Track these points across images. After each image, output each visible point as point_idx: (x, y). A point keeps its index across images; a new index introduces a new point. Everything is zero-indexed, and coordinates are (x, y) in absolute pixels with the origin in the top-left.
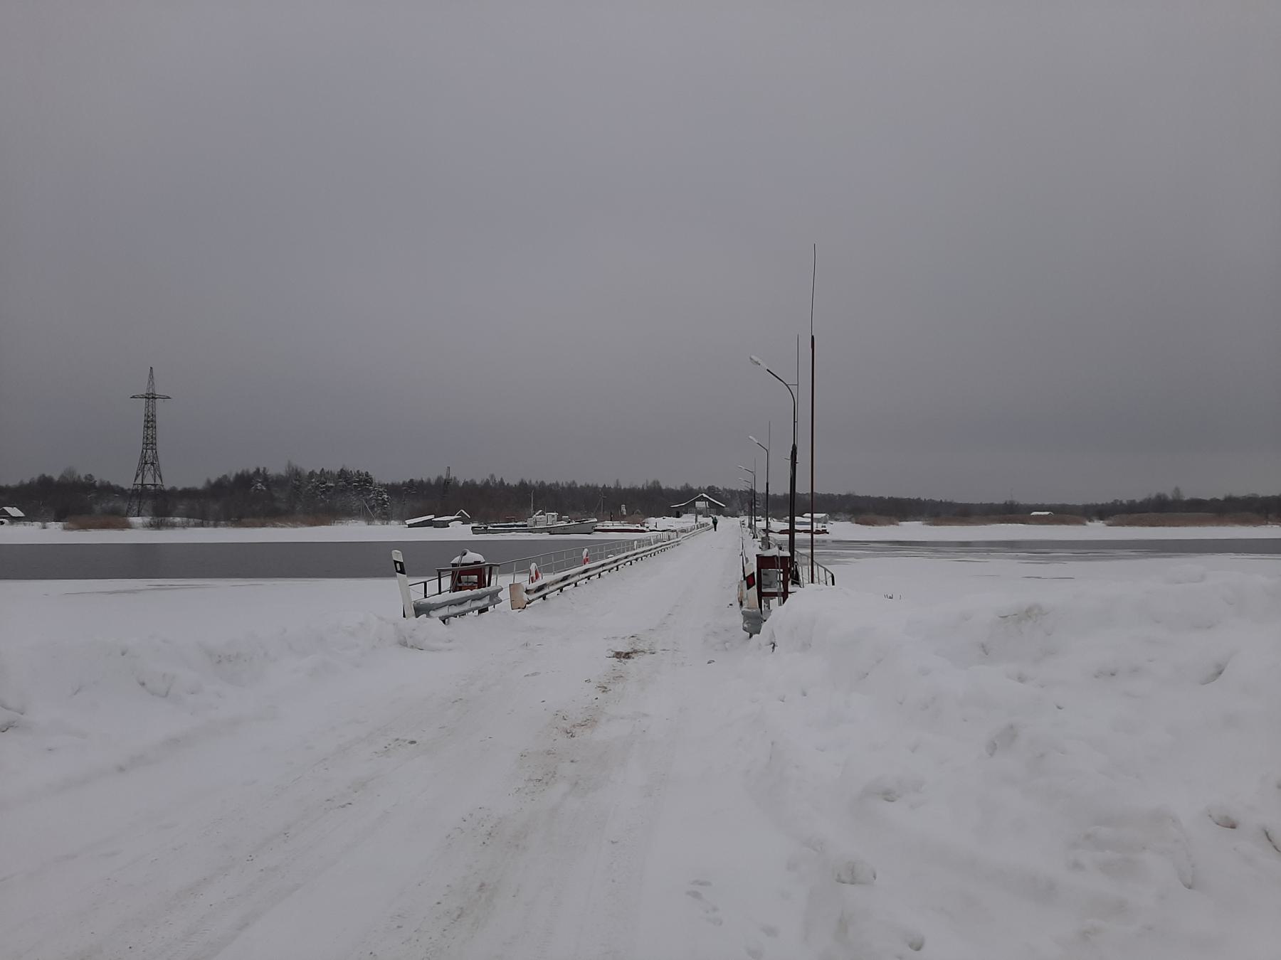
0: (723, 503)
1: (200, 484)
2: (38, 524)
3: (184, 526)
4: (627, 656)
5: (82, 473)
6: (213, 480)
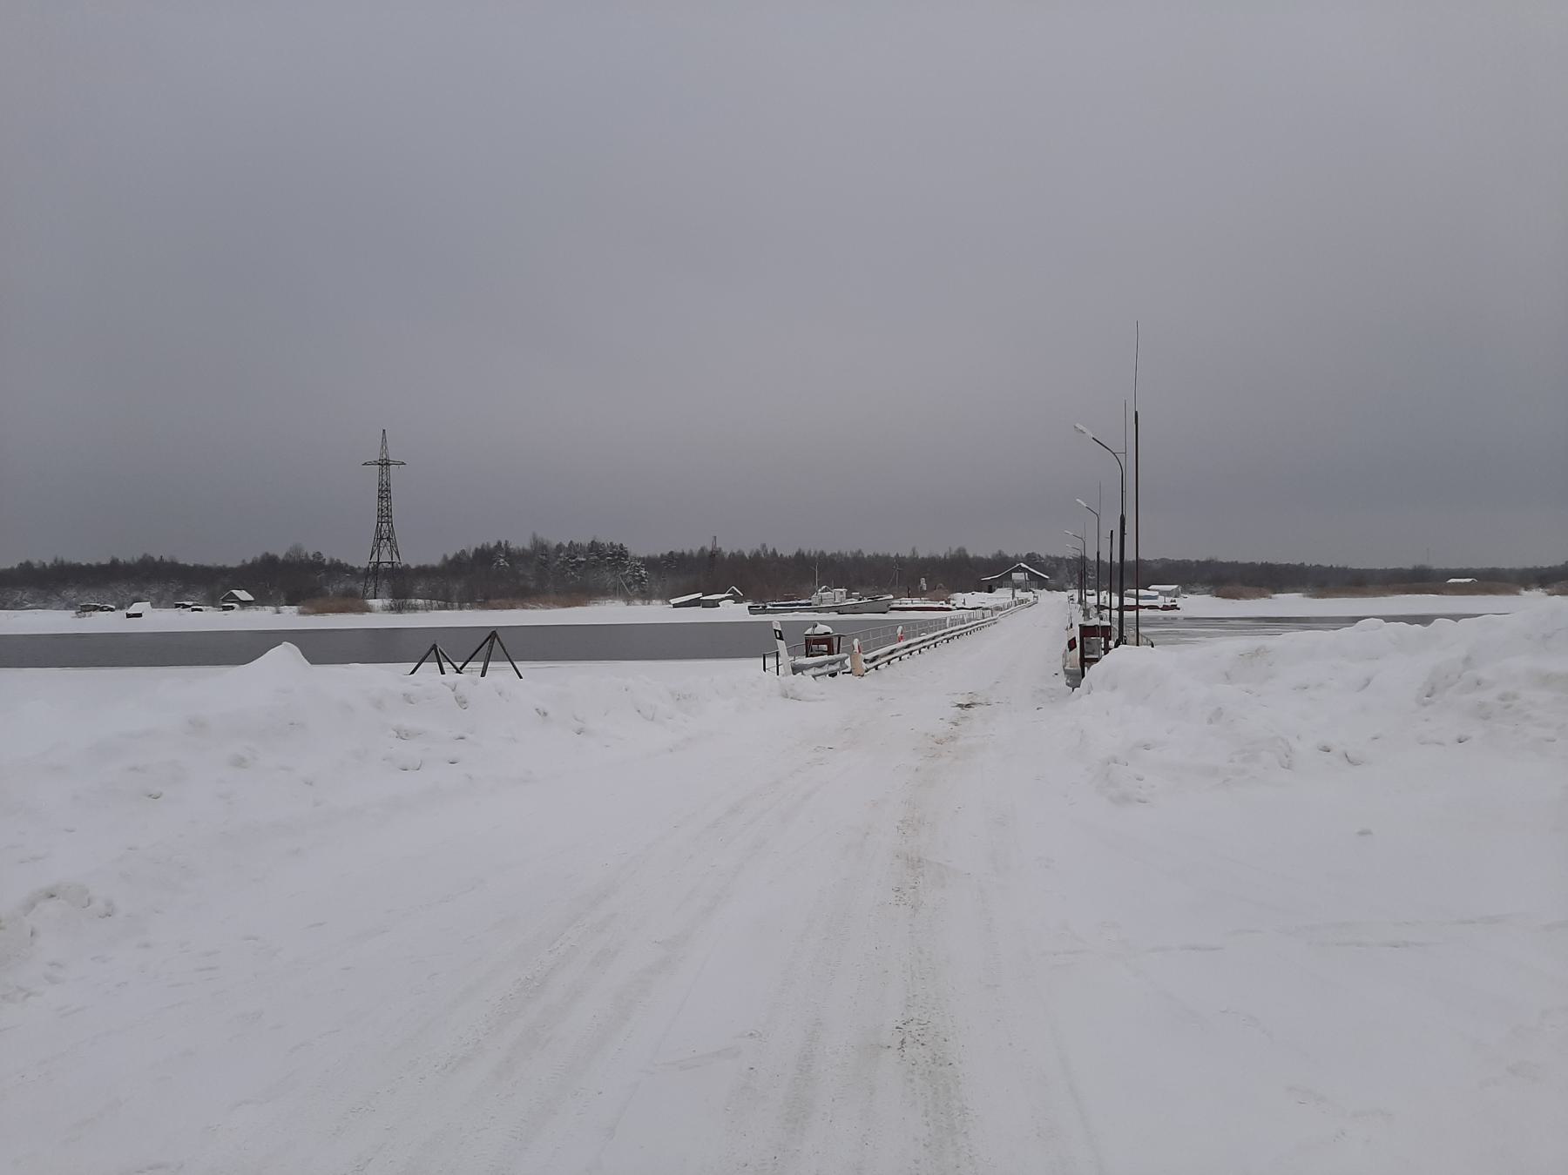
0: (1046, 573)
1: (436, 561)
2: (270, 610)
3: (427, 609)
4: (968, 706)
5: (310, 551)
6: (450, 557)
